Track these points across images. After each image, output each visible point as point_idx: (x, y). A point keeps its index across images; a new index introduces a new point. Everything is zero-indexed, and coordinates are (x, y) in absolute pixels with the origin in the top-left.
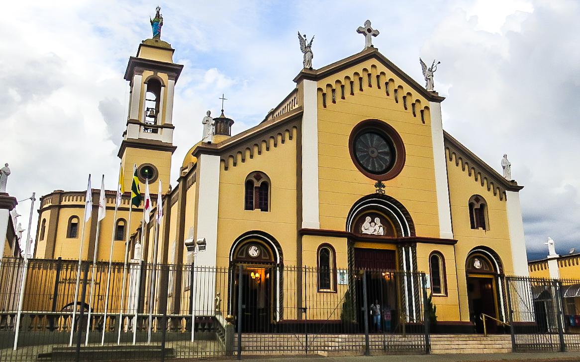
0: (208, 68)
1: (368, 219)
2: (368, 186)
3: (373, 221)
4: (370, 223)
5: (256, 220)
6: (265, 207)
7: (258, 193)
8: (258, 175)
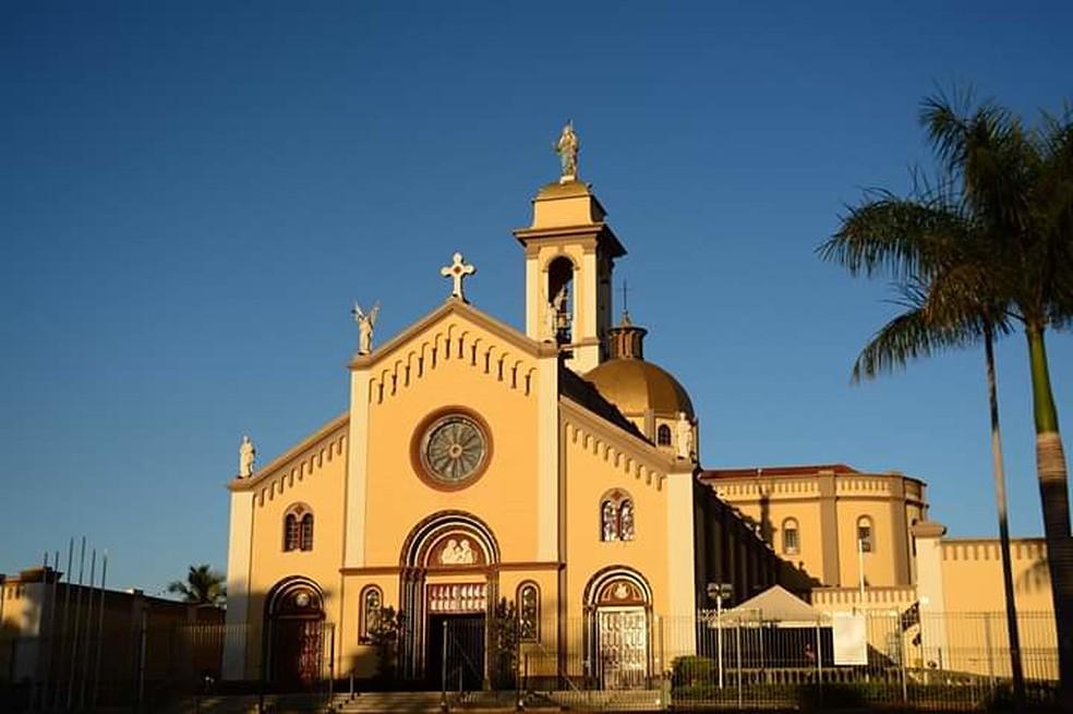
1: (452, 543)
2: (433, 502)
4: (454, 549)
6: (306, 547)
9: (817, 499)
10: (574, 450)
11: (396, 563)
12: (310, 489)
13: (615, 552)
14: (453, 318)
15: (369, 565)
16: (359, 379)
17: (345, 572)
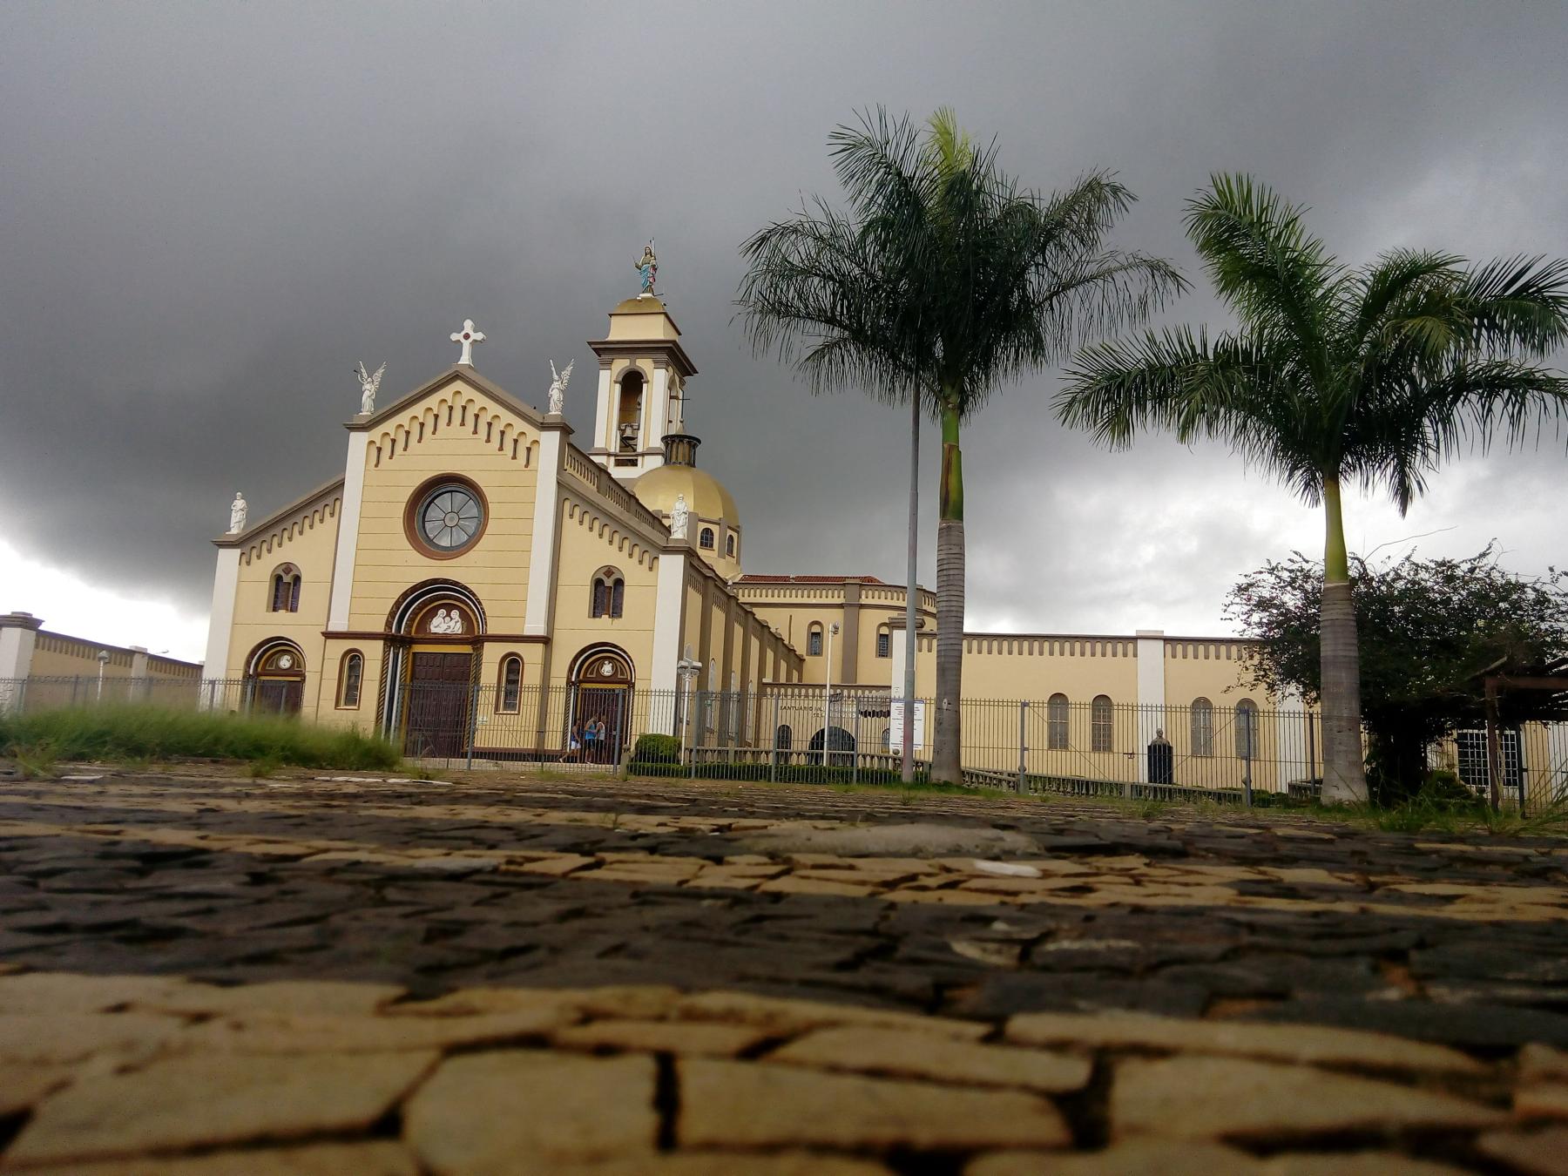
0: (1371, 780)
1: (442, 612)
2: (426, 569)
3: (448, 615)
5: (281, 624)
6: (616, 612)
7: (285, 590)
8: (288, 568)
9: (841, 606)
10: (570, 525)
11: (380, 628)
12: (298, 549)
13: (604, 630)
14: (458, 385)
15: (353, 629)
16: (358, 441)
17: (329, 635)
